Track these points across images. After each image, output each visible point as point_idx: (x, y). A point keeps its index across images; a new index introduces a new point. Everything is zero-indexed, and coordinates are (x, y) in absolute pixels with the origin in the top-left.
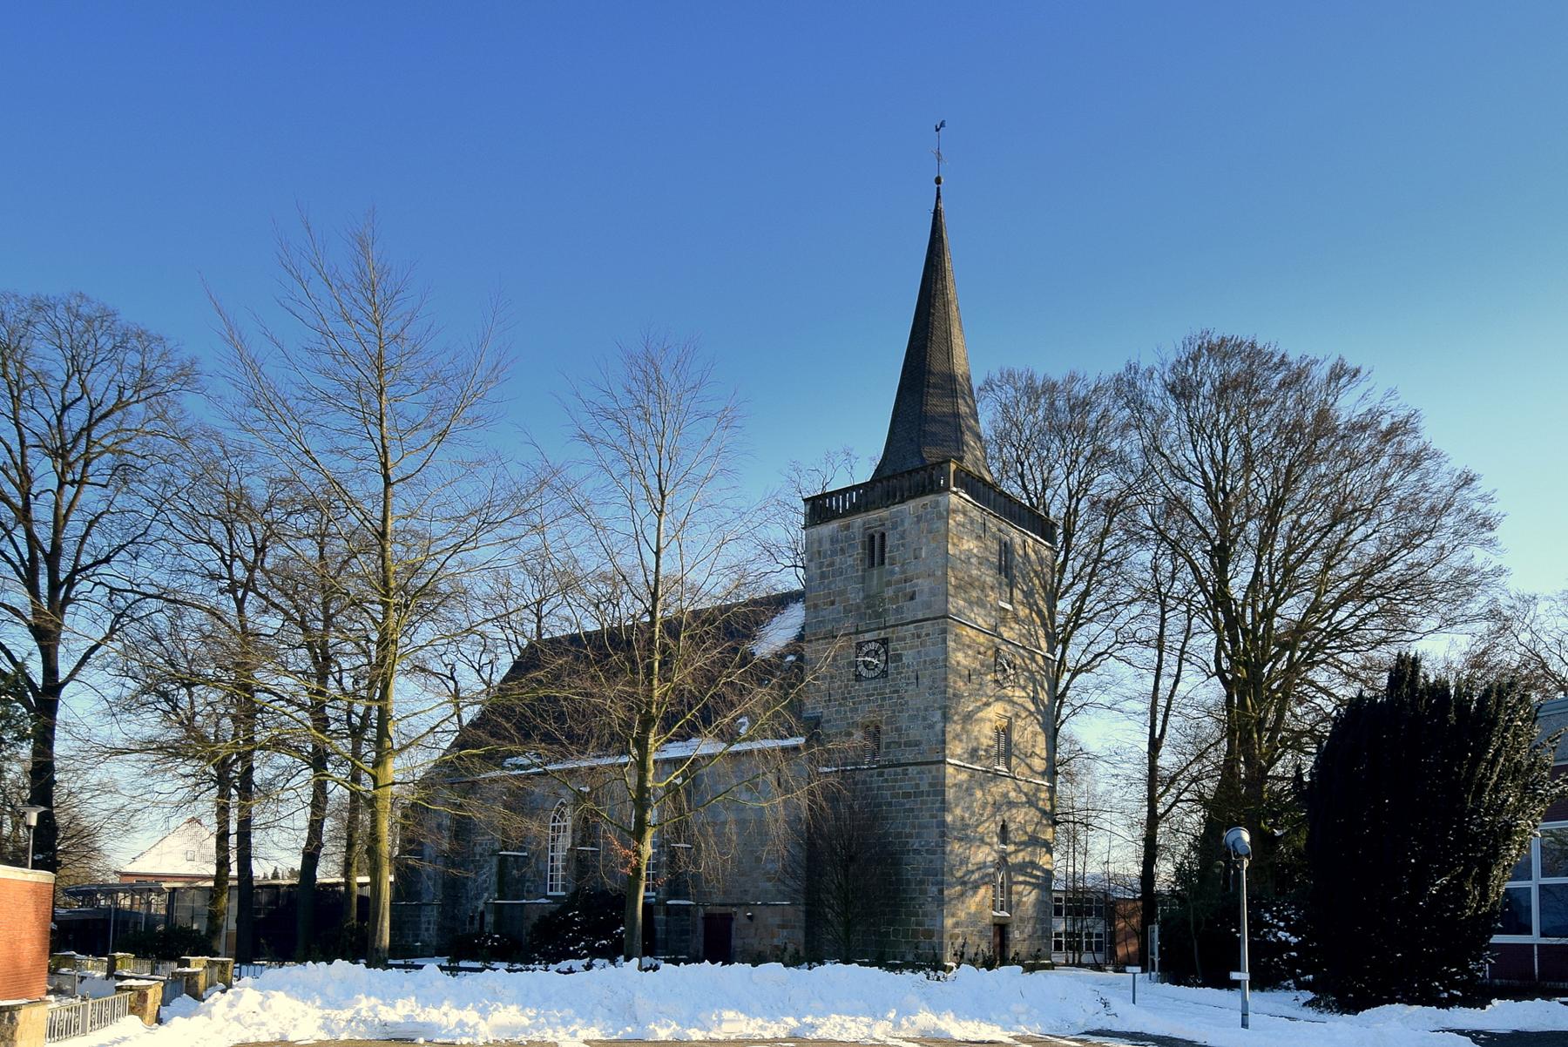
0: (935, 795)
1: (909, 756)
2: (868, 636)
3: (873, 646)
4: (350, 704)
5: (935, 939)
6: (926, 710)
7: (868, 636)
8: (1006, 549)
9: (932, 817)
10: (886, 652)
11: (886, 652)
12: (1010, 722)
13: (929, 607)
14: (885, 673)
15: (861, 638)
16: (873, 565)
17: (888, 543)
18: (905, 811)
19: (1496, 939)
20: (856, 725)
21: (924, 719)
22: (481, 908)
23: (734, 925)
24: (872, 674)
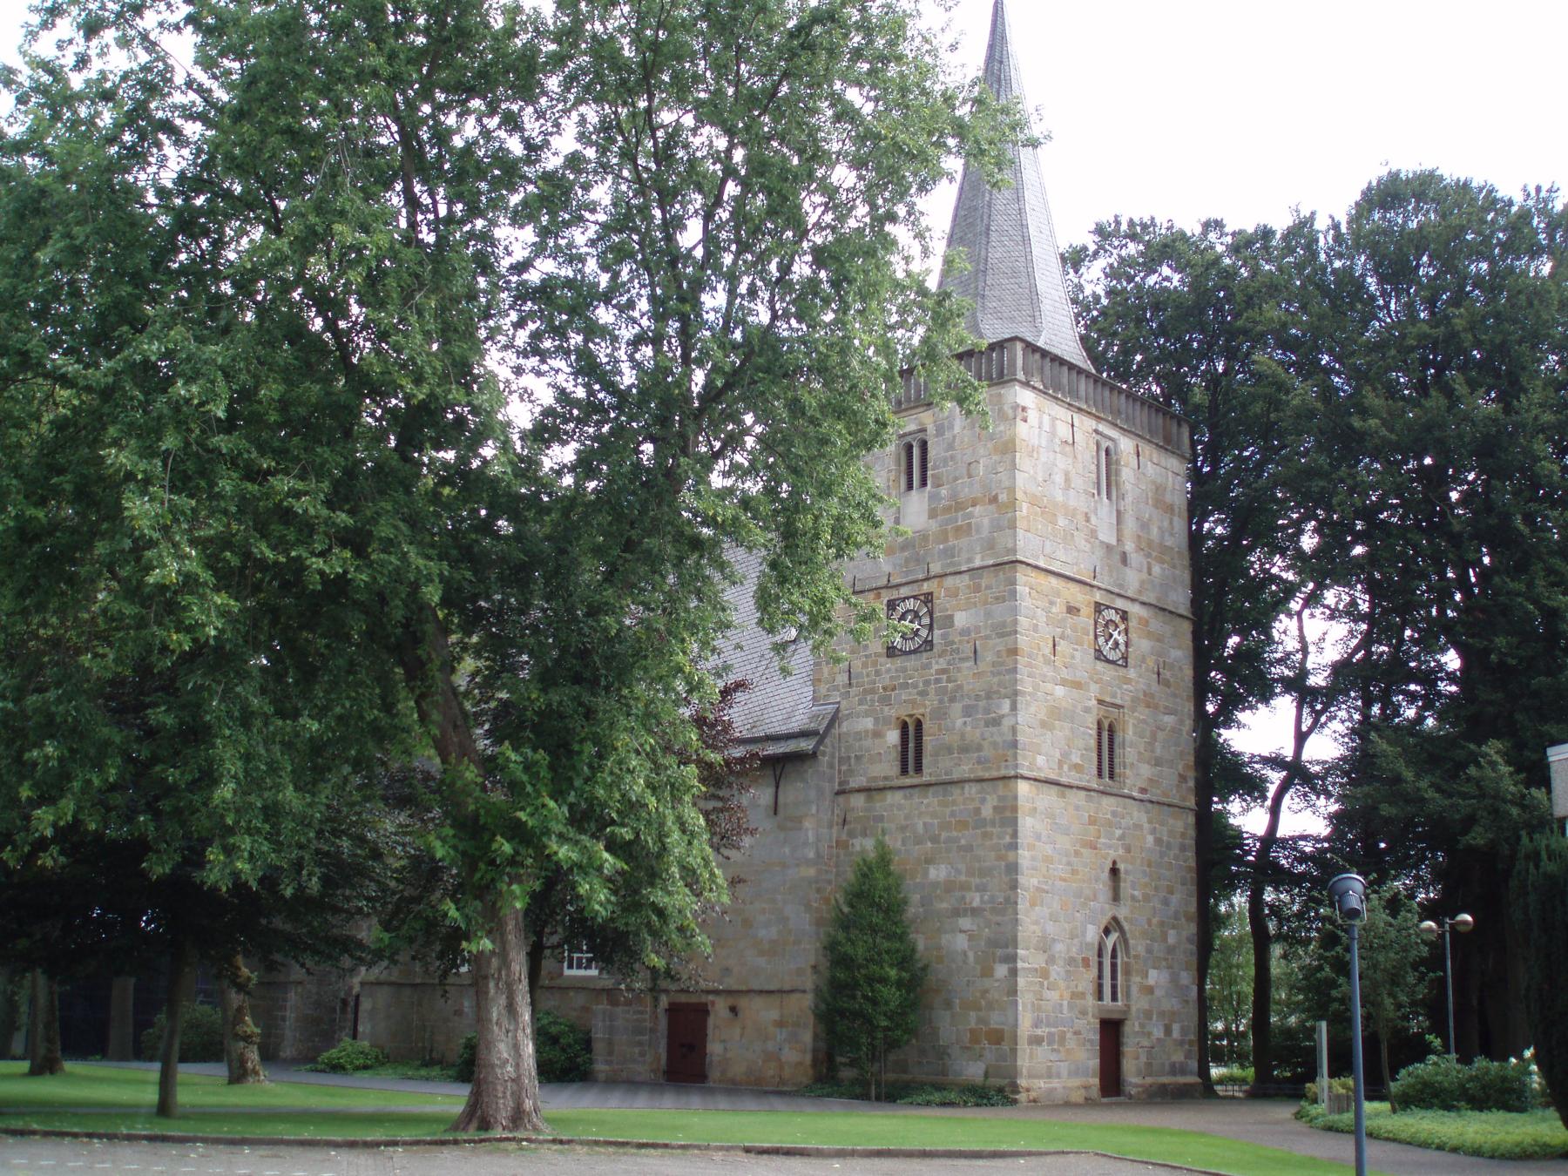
0: (1003, 825)
1: (965, 769)
2: (904, 591)
3: (910, 604)
4: (118, 105)
5: (1005, 1047)
6: (988, 697)
7: (904, 591)
8: (1110, 455)
9: (1000, 858)
10: (931, 613)
11: (931, 613)
12: (455, 892)
13: (992, 547)
14: (929, 644)
15: (894, 594)
16: (910, 487)
17: (932, 453)
18: (960, 848)
19: (1324, 1024)
20: (887, 721)
21: (987, 711)
22: (356, 989)
23: (711, 1021)
24: (910, 646)
